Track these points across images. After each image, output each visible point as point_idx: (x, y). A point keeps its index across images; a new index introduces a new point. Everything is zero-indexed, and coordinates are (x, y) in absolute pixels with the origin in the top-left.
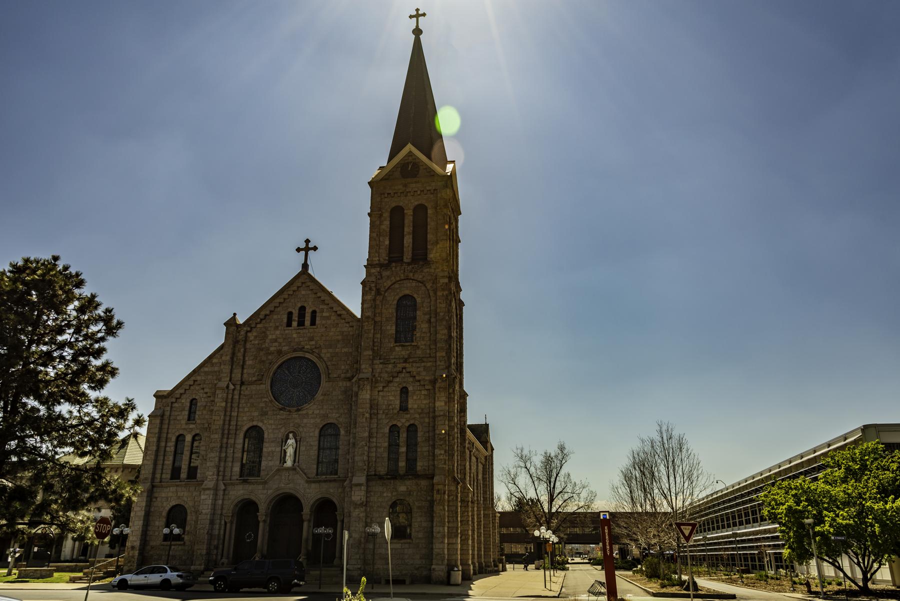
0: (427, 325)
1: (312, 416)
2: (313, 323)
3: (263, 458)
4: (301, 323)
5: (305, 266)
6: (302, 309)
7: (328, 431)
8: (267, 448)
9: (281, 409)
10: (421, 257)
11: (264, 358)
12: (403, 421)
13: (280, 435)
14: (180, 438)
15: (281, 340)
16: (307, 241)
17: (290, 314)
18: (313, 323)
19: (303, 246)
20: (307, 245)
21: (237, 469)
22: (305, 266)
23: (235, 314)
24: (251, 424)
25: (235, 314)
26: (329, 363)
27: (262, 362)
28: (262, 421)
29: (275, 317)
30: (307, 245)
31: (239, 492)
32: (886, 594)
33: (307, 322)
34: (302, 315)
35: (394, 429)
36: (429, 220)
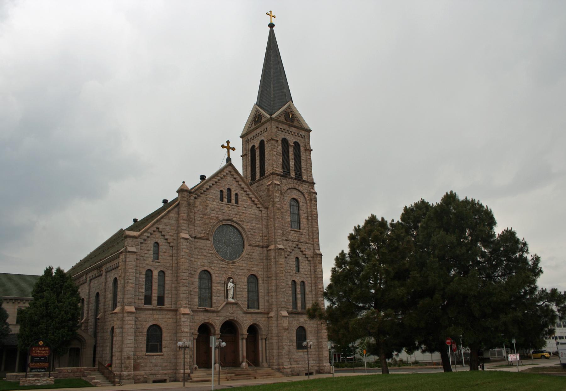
0: (306, 220)
1: (243, 267)
2: (237, 202)
3: (214, 294)
4: (229, 201)
5: (229, 160)
6: (229, 190)
7: (253, 279)
8: (215, 287)
9: (222, 261)
10: (299, 177)
11: (207, 221)
12: (298, 278)
13: (224, 279)
14: (149, 273)
15: (217, 210)
16: (223, 146)
17: (221, 191)
18: (237, 202)
19: (231, 145)
20: (225, 147)
21: (197, 300)
22: (229, 160)
23: (184, 182)
24: (203, 269)
25: (184, 182)
26: (249, 233)
27: (206, 224)
28: (210, 267)
29: (212, 191)
30: (225, 147)
31: (202, 318)
32: (114, 288)
33: (233, 201)
34: (229, 196)
35: (149, 273)
36: (301, 153)
